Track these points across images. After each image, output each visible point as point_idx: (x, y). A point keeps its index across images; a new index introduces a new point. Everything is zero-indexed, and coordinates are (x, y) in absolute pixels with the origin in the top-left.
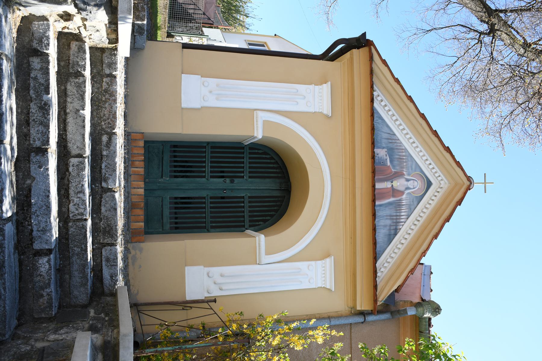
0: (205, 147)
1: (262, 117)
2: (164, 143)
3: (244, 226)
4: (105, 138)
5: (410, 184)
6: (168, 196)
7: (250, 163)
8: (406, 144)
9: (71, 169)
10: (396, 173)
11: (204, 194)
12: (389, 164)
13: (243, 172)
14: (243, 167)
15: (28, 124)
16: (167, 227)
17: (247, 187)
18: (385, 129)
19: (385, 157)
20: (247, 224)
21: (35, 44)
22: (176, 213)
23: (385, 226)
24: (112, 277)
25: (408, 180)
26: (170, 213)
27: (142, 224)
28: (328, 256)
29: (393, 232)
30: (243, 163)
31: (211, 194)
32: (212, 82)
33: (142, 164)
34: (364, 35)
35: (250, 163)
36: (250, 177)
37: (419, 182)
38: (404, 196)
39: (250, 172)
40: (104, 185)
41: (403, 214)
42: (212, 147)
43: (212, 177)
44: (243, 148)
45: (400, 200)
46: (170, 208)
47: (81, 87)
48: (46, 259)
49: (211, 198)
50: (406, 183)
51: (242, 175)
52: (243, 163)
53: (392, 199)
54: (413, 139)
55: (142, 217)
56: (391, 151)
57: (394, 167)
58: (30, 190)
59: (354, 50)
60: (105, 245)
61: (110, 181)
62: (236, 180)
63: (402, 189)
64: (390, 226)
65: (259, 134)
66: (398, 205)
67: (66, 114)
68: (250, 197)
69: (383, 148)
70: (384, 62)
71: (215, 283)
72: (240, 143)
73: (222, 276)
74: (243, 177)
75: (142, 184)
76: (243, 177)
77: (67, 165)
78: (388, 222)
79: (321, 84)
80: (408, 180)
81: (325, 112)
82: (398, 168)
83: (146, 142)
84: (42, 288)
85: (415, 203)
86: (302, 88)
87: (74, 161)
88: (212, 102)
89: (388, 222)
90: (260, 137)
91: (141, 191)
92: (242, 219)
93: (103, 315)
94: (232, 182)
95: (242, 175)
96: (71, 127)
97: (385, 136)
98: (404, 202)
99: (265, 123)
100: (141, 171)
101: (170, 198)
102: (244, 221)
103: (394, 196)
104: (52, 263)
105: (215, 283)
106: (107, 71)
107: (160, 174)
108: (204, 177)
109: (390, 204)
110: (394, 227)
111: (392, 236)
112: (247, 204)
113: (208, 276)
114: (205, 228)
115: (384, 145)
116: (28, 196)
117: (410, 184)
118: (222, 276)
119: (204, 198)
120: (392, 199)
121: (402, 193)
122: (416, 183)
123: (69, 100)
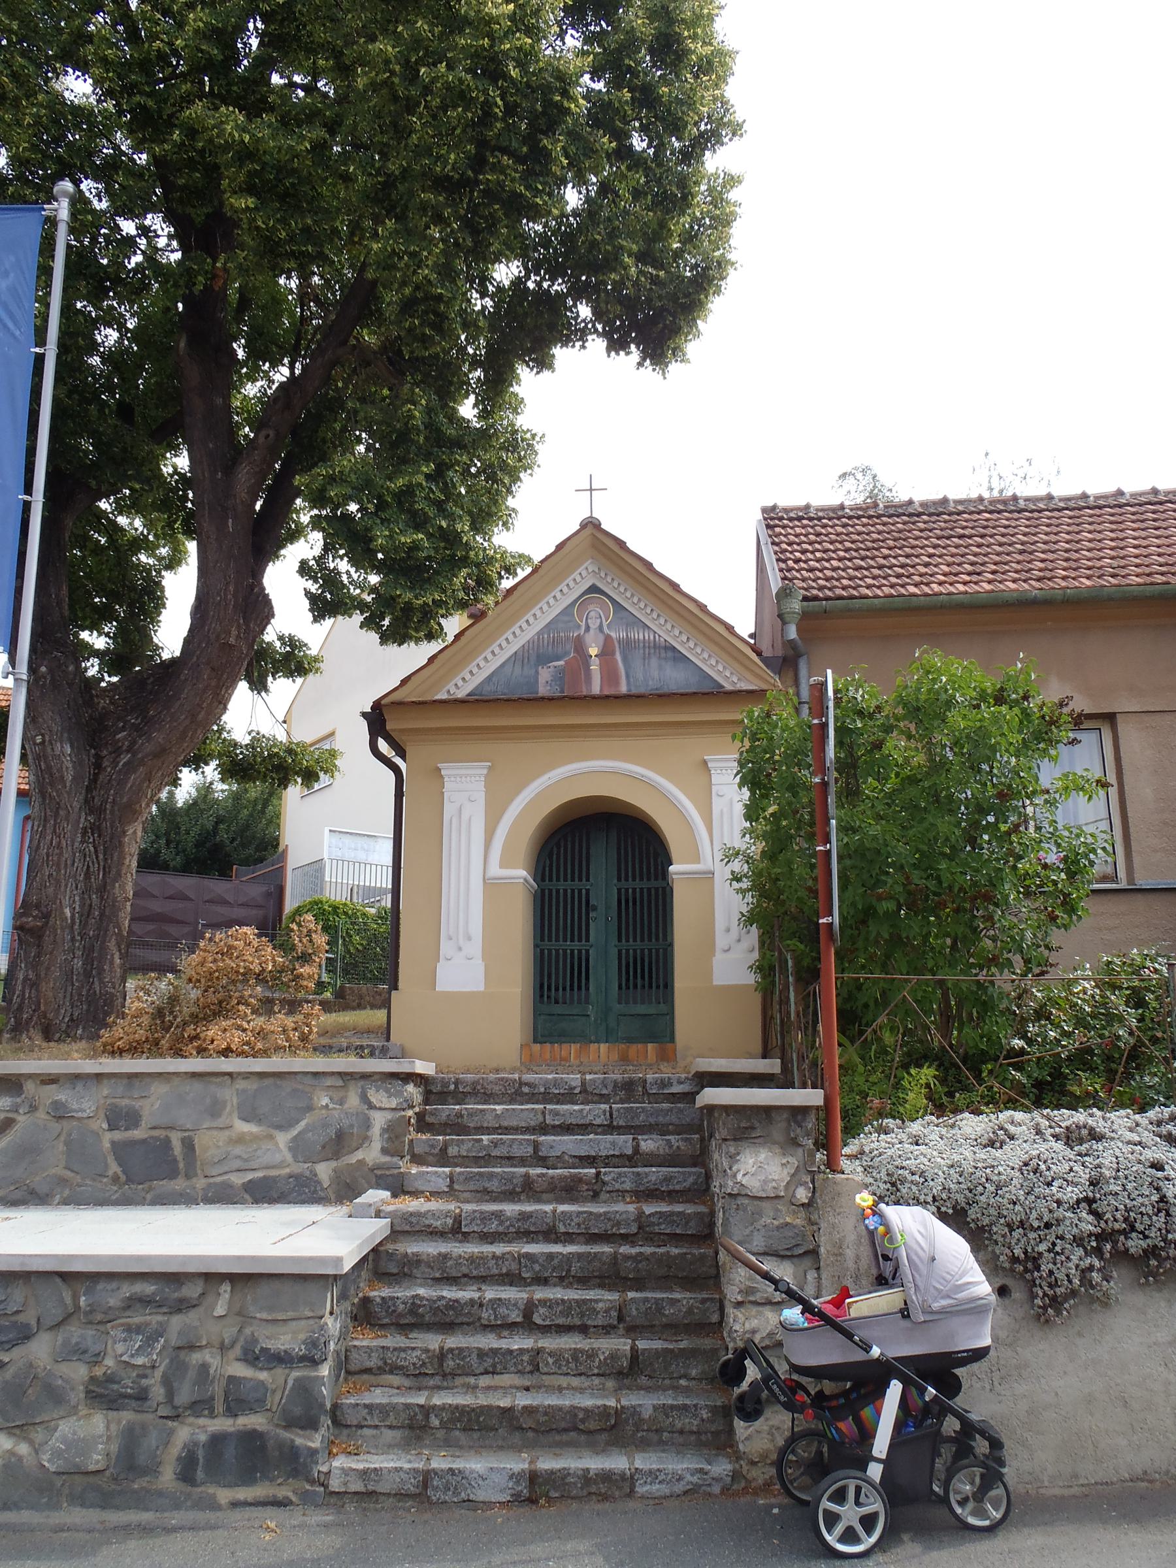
0: (542, 951)
1: (495, 870)
2: (537, 1013)
3: (664, 889)
4: (526, 1090)
5: (594, 624)
6: (618, 1008)
7: (565, 880)
8: (530, 633)
9: (557, 1123)
10: (576, 650)
11: (614, 952)
12: (562, 663)
13: (580, 891)
14: (573, 891)
15: (509, 1158)
16: (663, 1008)
17: (602, 884)
18: (508, 669)
19: (552, 669)
20: (659, 884)
21: (437, 1151)
22: (658, 987)
23: (660, 668)
24: (682, 1083)
25: (588, 628)
26: (643, 1003)
27: (650, 1046)
28: (705, 762)
29: (670, 654)
30: (565, 891)
31: (615, 941)
32: (446, 948)
33: (564, 1046)
34: (364, 715)
35: (565, 880)
36: (588, 880)
37: (591, 607)
38: (613, 634)
39: (580, 880)
40: (577, 1091)
41: (641, 637)
42: (542, 940)
43: (587, 940)
44: (543, 891)
45: (619, 642)
46: (635, 1002)
47: (472, 1114)
48: (642, 1143)
49: (620, 940)
50: (592, 631)
51: (584, 892)
52: (565, 891)
53: (618, 657)
54: (522, 623)
55: (640, 1046)
56: (543, 659)
57: (567, 653)
58: (575, 1157)
59: (388, 728)
60: (645, 1092)
61: (573, 1084)
62: (593, 902)
63: (601, 638)
64: (659, 658)
65: (521, 873)
66: (628, 646)
67: (500, 1127)
68: (619, 879)
69: (537, 672)
70: (404, 682)
71: (739, 941)
72: (535, 896)
73: (728, 930)
74: (588, 891)
75: (593, 1046)
76: (588, 891)
77: (554, 1127)
78: (654, 662)
79: (442, 777)
80: (588, 628)
81: (485, 771)
82: (568, 647)
83: (535, 1041)
84: (671, 1147)
85: (625, 614)
86: (449, 810)
87: (549, 1120)
88: (475, 948)
89: (654, 662)
90: (524, 873)
91: (603, 1047)
92: (653, 892)
93: (141, 994)
94: (595, 909)
95: (584, 892)
96: (514, 1123)
97: (518, 670)
98: (623, 635)
99: (502, 865)
100: (574, 1047)
101: (620, 1003)
102: (657, 889)
103: (613, 653)
104: (645, 1137)
105: (739, 941)
106: (452, 1087)
107: (584, 1018)
108: (587, 951)
109: (625, 659)
110: (663, 651)
111: (677, 655)
112: (631, 884)
113: (728, 950)
114: (665, 950)
115: (533, 671)
116: (581, 1158)
117: (594, 624)
118: (728, 930)
119: (620, 952)
120: (618, 657)
121: (608, 638)
122: (592, 614)
123: (485, 1125)
